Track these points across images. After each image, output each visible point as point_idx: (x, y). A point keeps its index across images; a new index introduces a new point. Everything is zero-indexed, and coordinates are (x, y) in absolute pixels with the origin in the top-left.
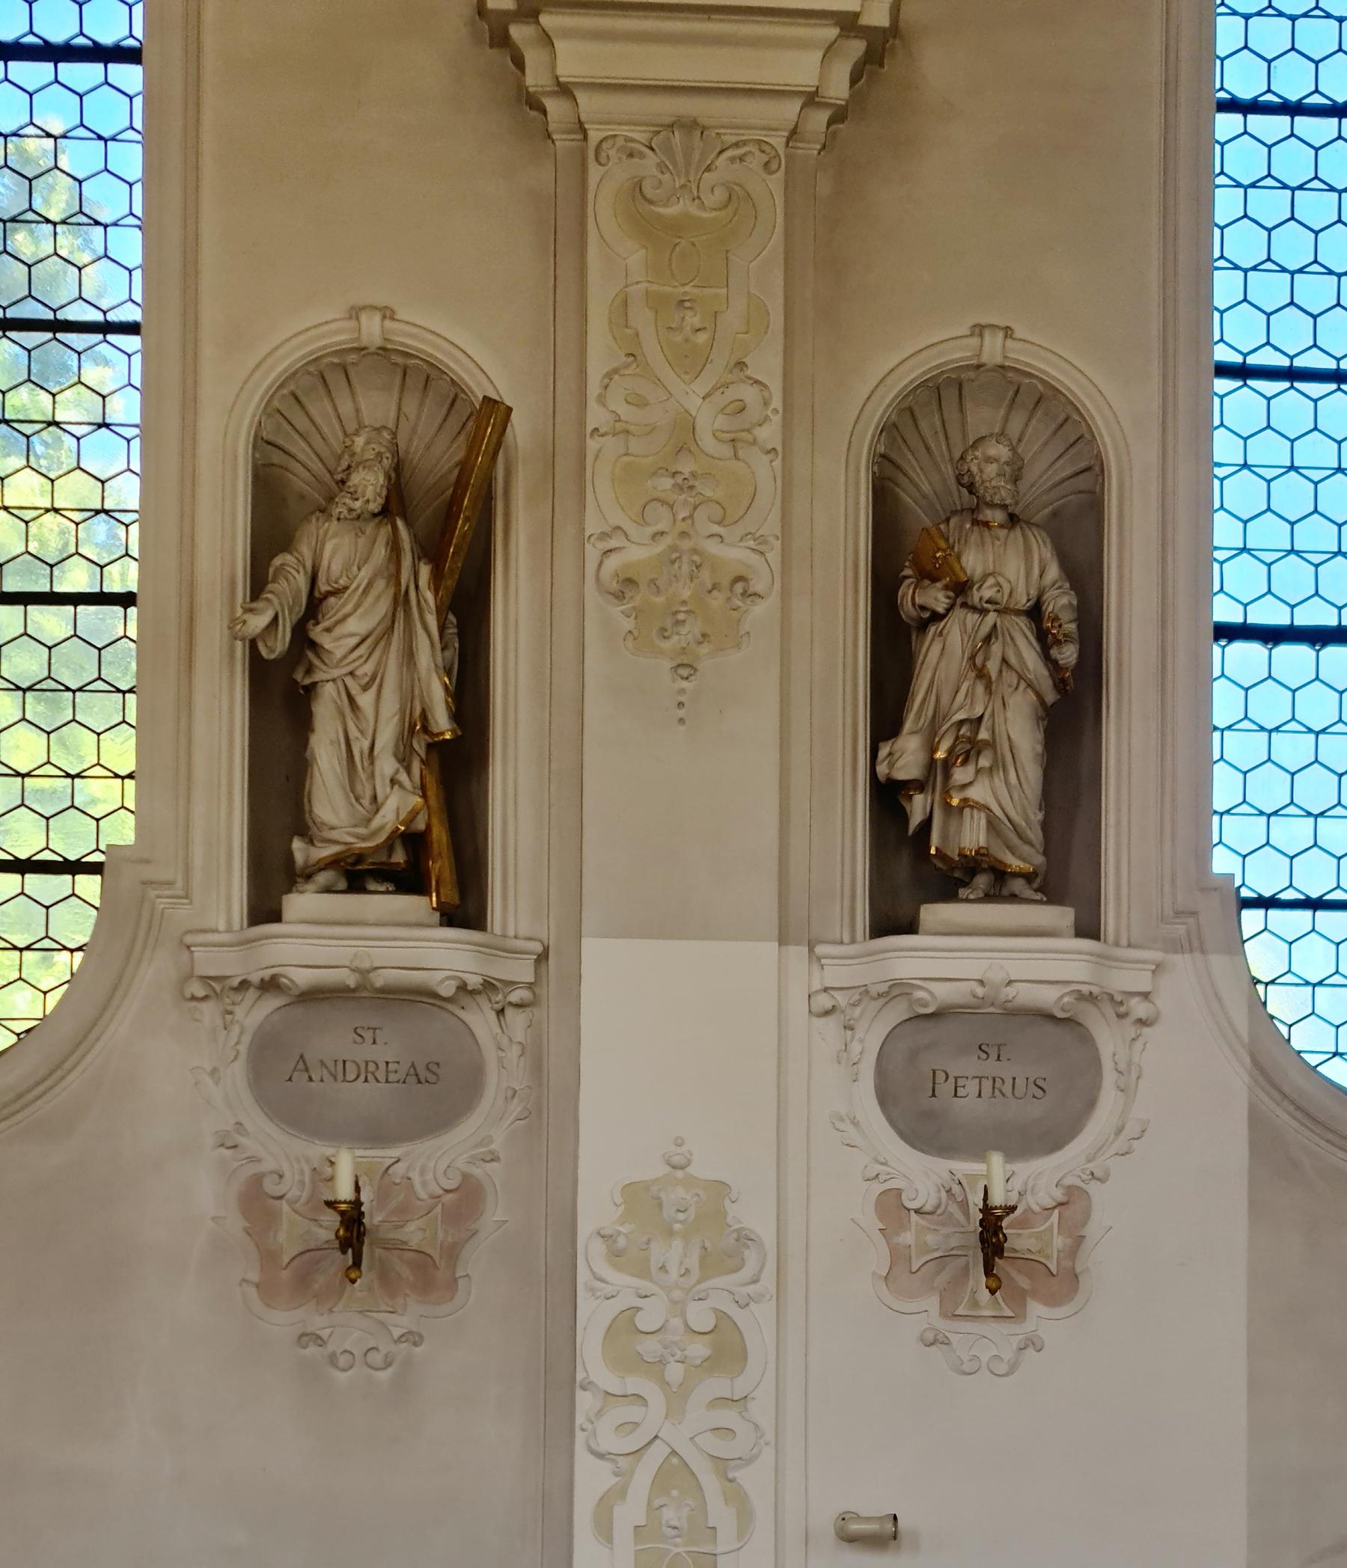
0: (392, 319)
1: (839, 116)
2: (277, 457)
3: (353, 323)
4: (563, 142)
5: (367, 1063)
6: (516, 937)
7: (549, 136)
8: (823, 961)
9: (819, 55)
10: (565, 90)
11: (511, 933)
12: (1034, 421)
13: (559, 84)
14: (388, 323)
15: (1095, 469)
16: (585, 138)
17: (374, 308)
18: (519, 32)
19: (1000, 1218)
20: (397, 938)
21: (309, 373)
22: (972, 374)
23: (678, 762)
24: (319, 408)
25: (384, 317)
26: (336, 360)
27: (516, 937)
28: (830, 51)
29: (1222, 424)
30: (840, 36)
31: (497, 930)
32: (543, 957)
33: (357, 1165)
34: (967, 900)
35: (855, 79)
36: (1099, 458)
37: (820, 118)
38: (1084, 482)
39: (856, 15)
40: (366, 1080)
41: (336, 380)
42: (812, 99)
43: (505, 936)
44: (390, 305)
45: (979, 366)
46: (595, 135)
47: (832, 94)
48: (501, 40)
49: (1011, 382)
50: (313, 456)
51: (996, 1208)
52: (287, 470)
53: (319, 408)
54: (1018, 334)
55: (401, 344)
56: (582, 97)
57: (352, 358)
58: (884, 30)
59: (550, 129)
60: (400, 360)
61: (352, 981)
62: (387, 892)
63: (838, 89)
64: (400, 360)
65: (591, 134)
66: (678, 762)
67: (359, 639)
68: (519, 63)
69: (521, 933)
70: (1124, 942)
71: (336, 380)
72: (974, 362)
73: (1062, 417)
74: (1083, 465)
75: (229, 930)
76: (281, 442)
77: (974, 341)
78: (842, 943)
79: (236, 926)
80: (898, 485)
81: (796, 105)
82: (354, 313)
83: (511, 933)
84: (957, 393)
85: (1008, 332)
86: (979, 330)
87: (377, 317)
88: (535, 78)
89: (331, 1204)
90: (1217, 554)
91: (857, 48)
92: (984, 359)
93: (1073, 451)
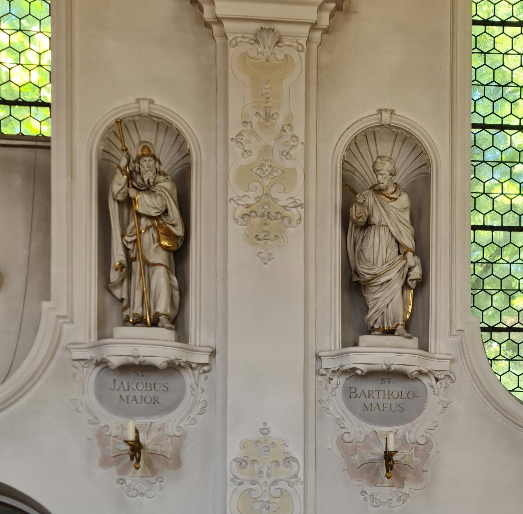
0: (153, 104)
1: (326, 31)
3: (137, 105)
4: (218, 40)
5: (154, 397)
6: (200, 346)
7: (213, 38)
8: (71, 350)
9: (316, 8)
10: (219, 21)
11: (198, 344)
12: (403, 148)
14: (151, 105)
15: (427, 164)
16: (227, 39)
17: (146, 99)
20: (156, 345)
25: (150, 103)
26: (131, 119)
27: (200, 346)
31: (433, 351)
32: (213, 354)
34: (375, 335)
35: (331, 16)
36: (428, 160)
37: (317, 35)
38: (185, 160)
40: (154, 403)
41: (371, 138)
42: (314, 27)
43: (195, 345)
45: (140, 115)
46: (230, 38)
49: (394, 132)
52: (111, 162)
54: (397, 112)
55: (396, 124)
56: (226, 24)
57: (377, 129)
59: (214, 35)
62: (379, 335)
63: (325, 21)
65: (228, 37)
68: (201, 9)
69: (202, 344)
70: (438, 352)
71: (371, 138)
72: (139, 114)
74: (423, 163)
75: (335, 350)
76: (350, 162)
78: (331, 350)
79: (338, 348)
80: (111, 162)
81: (307, 29)
82: (138, 101)
83: (198, 344)
84: (373, 136)
85: (392, 112)
86: (380, 111)
87: (147, 103)
88: (207, 15)
92: (383, 122)
93: (419, 158)
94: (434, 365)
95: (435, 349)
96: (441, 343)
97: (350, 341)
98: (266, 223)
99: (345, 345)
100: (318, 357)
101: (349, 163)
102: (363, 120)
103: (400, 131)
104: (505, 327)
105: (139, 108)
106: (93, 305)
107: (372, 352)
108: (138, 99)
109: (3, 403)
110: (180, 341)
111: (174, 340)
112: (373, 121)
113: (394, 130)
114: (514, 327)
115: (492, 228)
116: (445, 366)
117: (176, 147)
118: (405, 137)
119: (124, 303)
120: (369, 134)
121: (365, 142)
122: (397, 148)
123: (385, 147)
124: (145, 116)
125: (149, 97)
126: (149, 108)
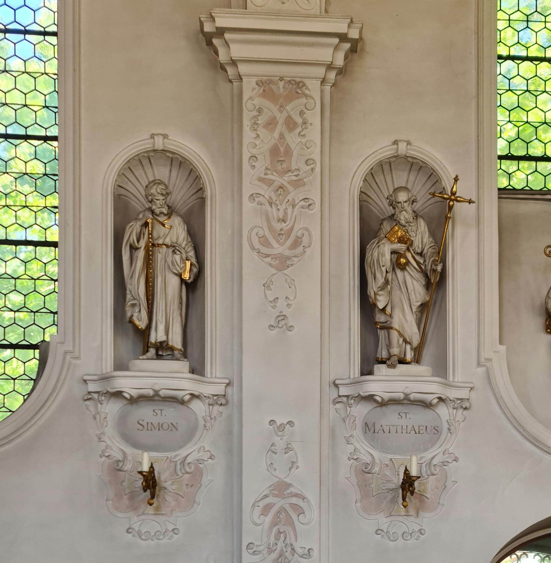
1: (341, 72)
2: (122, 192)
3: (152, 140)
10: (234, 63)
12: (180, 173)
13: (232, 60)
17: (161, 134)
18: (215, 41)
19: (414, 481)
20: (169, 375)
21: (135, 160)
22: (394, 159)
23: (282, 317)
24: (139, 172)
28: (336, 48)
29: (501, 10)
30: (339, 42)
31: (209, 376)
33: (150, 458)
35: (346, 58)
37: (332, 75)
39: (346, 34)
42: (330, 67)
44: (166, 133)
47: (337, 64)
48: (209, 43)
50: (136, 191)
51: (413, 477)
53: (139, 172)
57: (392, 160)
58: (357, 39)
60: (170, 155)
61: (151, 393)
63: (340, 61)
64: (170, 155)
66: (282, 317)
67: (153, 257)
68: (216, 53)
69: (218, 376)
71: (145, 162)
73: (430, 173)
77: (395, 146)
82: (152, 136)
88: (223, 57)
89: (141, 473)
90: (499, 123)
91: (347, 46)
92: (399, 153)
94: (452, 394)
95: (211, 374)
96: (215, 368)
97: (367, 370)
98: (284, 251)
99: (362, 374)
100: (336, 386)
101: (123, 188)
102: (378, 152)
103: (175, 156)
104: (8, 343)
105: (154, 144)
106: (451, 342)
107: (385, 382)
108: (152, 134)
109: (2, 439)
110: (193, 373)
111: (188, 371)
112: (388, 152)
113: (409, 159)
114: (20, 343)
115: (36, 244)
116: (463, 394)
117: (191, 180)
118: (416, 165)
119: (143, 335)
120: (386, 166)
121: (381, 172)
122: (412, 178)
123: (401, 178)
124: (402, 157)
125: (163, 133)
126: (164, 144)
